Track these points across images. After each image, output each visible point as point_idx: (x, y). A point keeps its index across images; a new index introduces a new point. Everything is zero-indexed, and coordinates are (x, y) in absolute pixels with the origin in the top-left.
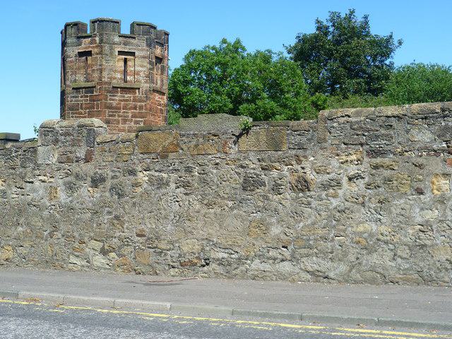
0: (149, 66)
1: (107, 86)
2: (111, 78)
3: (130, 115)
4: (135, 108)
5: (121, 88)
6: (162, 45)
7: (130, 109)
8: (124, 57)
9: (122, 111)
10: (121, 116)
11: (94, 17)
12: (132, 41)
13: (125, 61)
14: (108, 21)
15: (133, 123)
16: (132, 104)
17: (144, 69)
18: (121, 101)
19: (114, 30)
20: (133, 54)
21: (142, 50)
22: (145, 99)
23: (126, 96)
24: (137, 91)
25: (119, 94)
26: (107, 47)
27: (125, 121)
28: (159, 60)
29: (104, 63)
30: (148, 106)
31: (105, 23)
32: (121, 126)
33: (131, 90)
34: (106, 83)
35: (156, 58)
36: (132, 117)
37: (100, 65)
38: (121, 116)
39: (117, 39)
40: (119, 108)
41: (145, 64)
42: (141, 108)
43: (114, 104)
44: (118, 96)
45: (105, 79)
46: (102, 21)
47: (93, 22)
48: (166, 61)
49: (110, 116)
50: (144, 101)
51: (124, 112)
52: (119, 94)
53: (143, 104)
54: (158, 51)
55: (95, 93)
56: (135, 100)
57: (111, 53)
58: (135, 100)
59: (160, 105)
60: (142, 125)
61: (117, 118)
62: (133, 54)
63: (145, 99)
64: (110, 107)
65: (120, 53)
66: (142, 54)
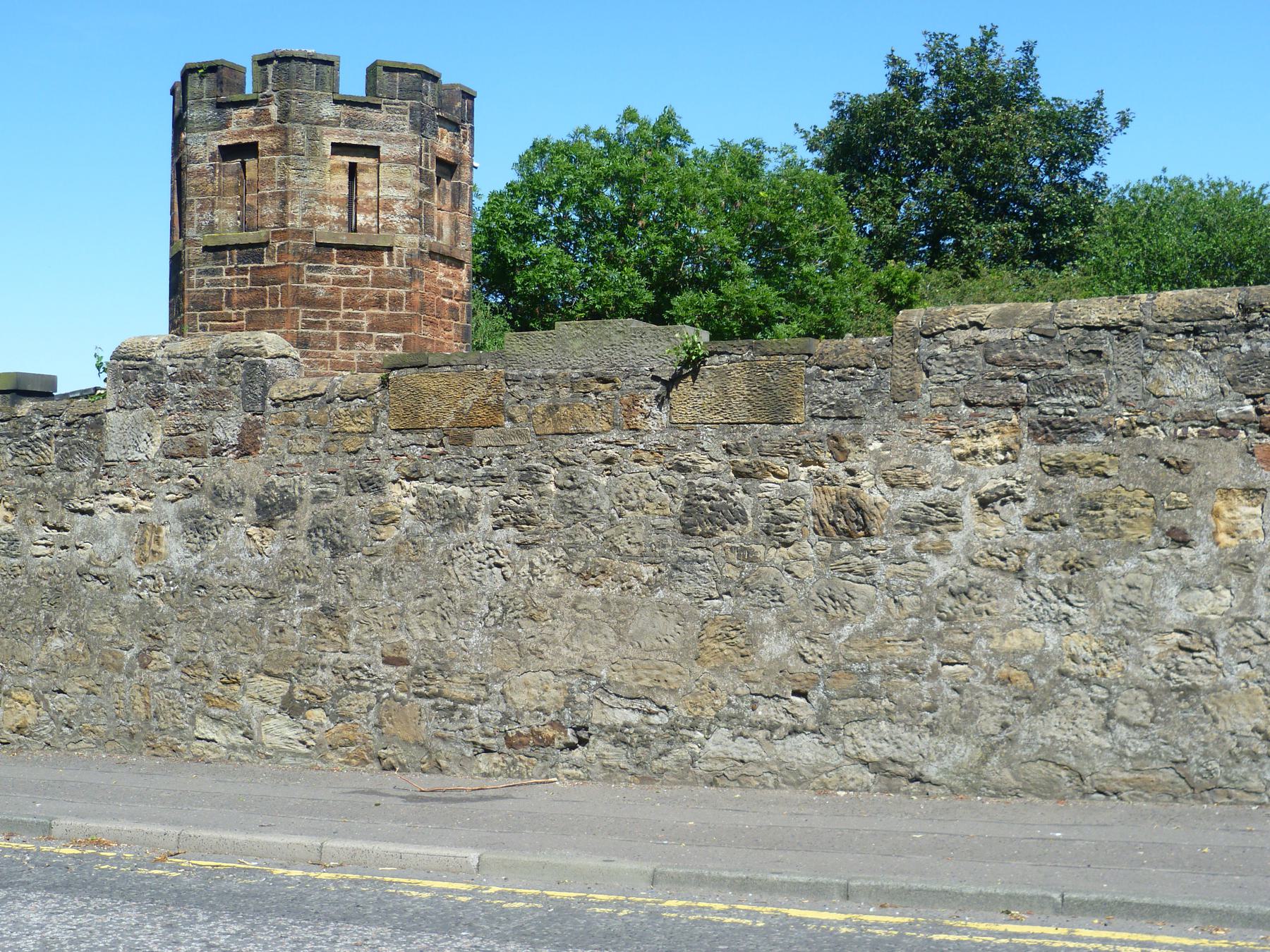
0: (418, 185)
1: (300, 242)
2: (310, 220)
3: (366, 323)
4: (379, 304)
5: (339, 247)
6: (455, 126)
7: (366, 305)
8: (347, 159)
9: (343, 311)
10: (340, 327)
11: (265, 49)
12: (371, 114)
13: (353, 170)
14: (304, 60)
15: (373, 346)
16: (370, 291)
17: (405, 194)
18: (340, 282)
19: (320, 84)
20: (373, 152)
21: (401, 140)
22: (407, 279)
23: (354, 269)
24: (385, 255)
25: (335, 265)
26: (299, 134)
27: (350, 340)
28: (448, 168)
29: (292, 178)
30: (417, 299)
31: (294, 65)
32: (339, 353)
33: (370, 252)
34: (297, 233)
35: (440, 162)
36: (372, 327)
37: (282, 183)
38: (340, 327)
39: (328, 110)
40: (335, 304)
41: (408, 180)
42: (396, 302)
43: (321, 291)
44: (333, 270)
45: (297, 223)
46: (285, 59)
47: (263, 62)
48: (465, 172)
49: (309, 325)
50: (405, 284)
51: (348, 315)
52: (335, 265)
53: (403, 292)
54: (444, 144)
55: (267, 263)
56: (378, 282)
57: (313, 151)
58: (378, 282)
59: (449, 295)
60: (399, 350)
61: (328, 331)
62: (373, 152)
63: (407, 279)
64: (308, 301)
65: (338, 148)
66: (401, 150)
